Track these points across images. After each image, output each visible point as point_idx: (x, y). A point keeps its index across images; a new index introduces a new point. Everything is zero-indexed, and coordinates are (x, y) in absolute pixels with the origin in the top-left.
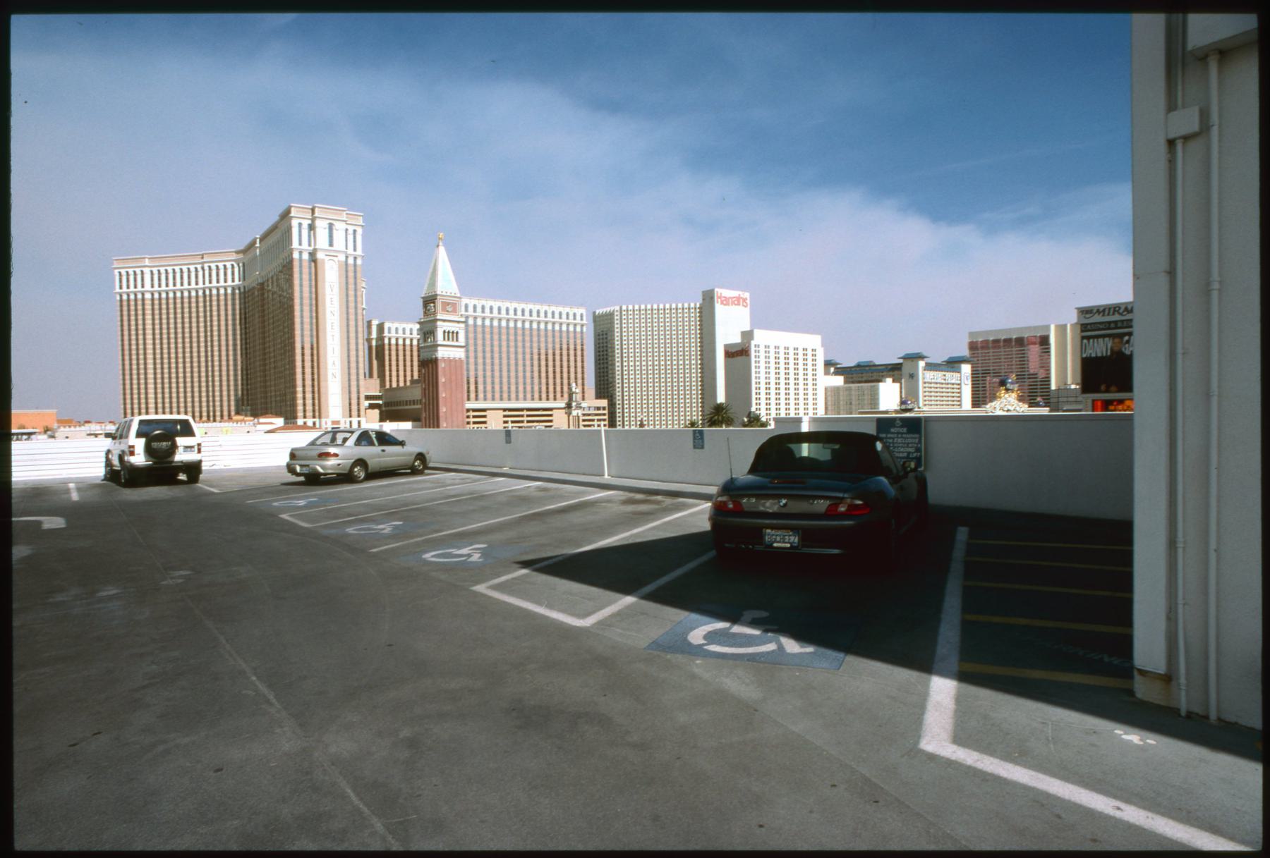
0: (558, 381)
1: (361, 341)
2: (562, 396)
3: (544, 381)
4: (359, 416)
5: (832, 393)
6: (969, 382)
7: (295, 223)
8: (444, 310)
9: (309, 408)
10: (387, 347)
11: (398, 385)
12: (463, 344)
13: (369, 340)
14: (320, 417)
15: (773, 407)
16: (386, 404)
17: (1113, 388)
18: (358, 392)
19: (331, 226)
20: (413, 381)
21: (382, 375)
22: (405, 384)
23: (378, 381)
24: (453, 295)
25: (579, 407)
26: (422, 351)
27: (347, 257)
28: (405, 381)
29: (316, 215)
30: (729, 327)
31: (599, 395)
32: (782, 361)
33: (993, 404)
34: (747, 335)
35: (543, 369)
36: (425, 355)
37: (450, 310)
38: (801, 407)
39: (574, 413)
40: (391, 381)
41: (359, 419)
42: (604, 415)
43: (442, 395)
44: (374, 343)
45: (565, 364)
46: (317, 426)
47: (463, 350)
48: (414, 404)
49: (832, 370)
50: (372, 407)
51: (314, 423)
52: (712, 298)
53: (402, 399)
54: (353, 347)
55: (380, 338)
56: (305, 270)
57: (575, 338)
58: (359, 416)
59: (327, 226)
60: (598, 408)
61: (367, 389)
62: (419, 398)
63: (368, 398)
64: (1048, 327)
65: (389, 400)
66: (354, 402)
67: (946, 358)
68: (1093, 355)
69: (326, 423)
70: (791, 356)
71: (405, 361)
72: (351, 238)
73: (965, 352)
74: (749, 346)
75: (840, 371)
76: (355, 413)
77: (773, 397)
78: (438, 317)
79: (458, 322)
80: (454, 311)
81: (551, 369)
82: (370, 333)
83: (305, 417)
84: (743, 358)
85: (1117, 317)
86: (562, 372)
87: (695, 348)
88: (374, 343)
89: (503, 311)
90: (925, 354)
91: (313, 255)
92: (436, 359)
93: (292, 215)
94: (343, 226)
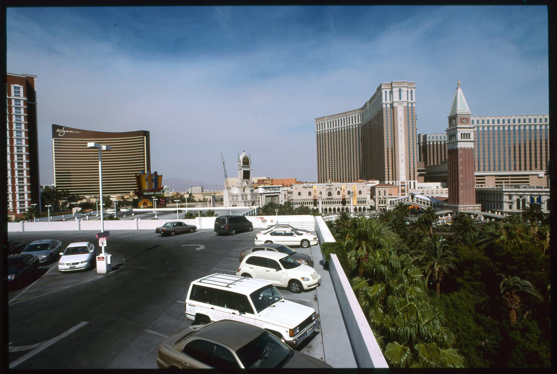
0: (528, 159)
1: (415, 143)
2: (536, 167)
4: (414, 180)
7: (383, 91)
8: (462, 122)
10: (428, 146)
12: (473, 140)
14: (396, 180)
18: (414, 168)
20: (441, 162)
23: (424, 163)
24: (467, 113)
28: (437, 162)
36: (452, 147)
40: (430, 162)
41: (414, 181)
44: (422, 145)
46: (394, 184)
47: (473, 143)
48: (442, 173)
50: (420, 175)
51: (393, 183)
55: (425, 142)
56: (389, 112)
61: (418, 167)
62: (447, 170)
69: (398, 183)
72: (410, 94)
76: (412, 178)
78: (458, 126)
79: (470, 128)
82: (419, 140)
83: (389, 180)
88: (422, 145)
91: (392, 105)
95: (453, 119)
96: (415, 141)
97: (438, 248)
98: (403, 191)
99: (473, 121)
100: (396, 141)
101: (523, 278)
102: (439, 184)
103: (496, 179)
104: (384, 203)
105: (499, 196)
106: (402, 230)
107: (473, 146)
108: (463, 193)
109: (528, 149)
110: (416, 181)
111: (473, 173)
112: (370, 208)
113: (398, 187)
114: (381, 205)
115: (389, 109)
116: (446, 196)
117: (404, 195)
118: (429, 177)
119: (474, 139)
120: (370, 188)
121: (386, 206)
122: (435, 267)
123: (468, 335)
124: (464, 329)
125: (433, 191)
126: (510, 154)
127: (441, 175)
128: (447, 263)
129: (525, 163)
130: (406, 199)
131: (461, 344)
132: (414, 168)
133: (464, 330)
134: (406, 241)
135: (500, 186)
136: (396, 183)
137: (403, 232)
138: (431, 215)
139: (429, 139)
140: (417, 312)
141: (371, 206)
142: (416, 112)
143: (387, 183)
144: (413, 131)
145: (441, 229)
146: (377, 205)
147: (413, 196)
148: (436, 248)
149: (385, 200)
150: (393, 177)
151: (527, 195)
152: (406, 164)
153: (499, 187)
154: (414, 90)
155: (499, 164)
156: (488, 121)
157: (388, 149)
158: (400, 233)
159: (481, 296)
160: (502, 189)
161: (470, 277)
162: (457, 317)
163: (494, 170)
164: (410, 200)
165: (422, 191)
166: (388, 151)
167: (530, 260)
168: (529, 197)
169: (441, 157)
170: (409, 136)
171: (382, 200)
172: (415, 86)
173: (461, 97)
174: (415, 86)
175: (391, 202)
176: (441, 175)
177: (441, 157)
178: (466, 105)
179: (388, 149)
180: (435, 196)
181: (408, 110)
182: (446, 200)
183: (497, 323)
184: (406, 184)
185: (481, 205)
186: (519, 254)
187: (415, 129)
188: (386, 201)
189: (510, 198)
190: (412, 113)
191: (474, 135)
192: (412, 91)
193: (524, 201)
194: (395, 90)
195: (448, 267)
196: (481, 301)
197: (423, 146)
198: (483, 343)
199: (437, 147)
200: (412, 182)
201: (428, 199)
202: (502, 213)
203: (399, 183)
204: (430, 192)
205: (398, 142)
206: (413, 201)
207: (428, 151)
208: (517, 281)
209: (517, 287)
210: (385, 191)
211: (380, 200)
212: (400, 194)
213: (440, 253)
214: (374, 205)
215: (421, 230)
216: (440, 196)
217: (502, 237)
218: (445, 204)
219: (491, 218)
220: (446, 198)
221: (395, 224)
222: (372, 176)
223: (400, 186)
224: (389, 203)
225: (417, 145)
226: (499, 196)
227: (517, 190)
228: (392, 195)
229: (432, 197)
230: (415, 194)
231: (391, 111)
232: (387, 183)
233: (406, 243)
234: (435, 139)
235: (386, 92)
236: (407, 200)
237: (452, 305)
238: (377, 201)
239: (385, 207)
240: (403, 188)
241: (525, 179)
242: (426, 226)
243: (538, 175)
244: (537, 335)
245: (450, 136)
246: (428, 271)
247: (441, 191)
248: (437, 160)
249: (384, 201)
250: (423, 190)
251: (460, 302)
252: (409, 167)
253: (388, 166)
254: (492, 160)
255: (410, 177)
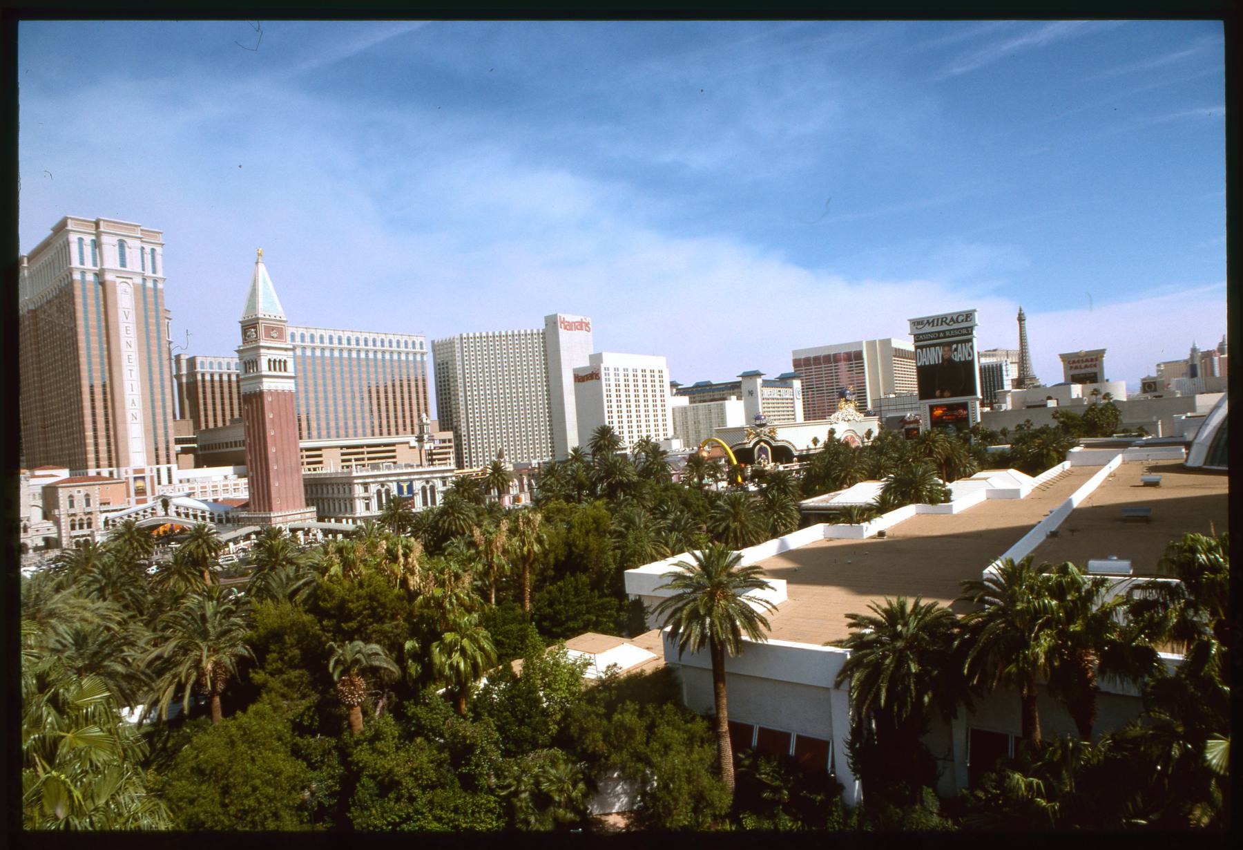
0: (392, 414)
1: (167, 377)
2: (405, 430)
3: (384, 414)
4: (169, 462)
5: (680, 413)
6: (801, 397)
7: (73, 238)
8: (268, 335)
9: (103, 455)
10: (200, 384)
11: (216, 425)
12: (293, 375)
13: (178, 377)
14: (118, 466)
15: (635, 429)
16: (203, 447)
17: (947, 393)
18: (166, 435)
19: (122, 244)
20: (233, 420)
21: (195, 417)
22: (224, 424)
23: (191, 422)
24: (278, 318)
25: (432, 439)
26: (241, 383)
27: (144, 280)
28: (224, 421)
29: (102, 229)
30: (574, 355)
31: (444, 427)
32: (631, 383)
33: (836, 414)
34: (596, 358)
35: (383, 402)
36: (246, 388)
37: (275, 335)
38: (652, 428)
39: (427, 446)
40: (207, 421)
42: (450, 447)
43: (271, 433)
44: (184, 380)
45: (406, 396)
46: (115, 476)
47: (293, 381)
48: (236, 446)
49: (674, 391)
50: (184, 451)
51: (111, 473)
52: (555, 323)
53: (217, 441)
54: (157, 382)
55: (192, 373)
56: (91, 295)
57: (415, 368)
58: (169, 462)
59: (117, 243)
60: (444, 441)
61: (177, 431)
62: (243, 438)
63: (178, 441)
64: (861, 343)
65: (204, 443)
66: (162, 446)
67: (778, 375)
68: (927, 363)
69: (126, 472)
70: (640, 378)
71: (214, 404)
72: (148, 258)
73: (790, 369)
74: (599, 369)
75: (682, 392)
76: (163, 458)
77: (634, 419)
78: (261, 344)
79: (286, 349)
80: (281, 336)
81: (391, 402)
82: (179, 368)
84: (594, 381)
85: (945, 327)
86: (403, 405)
87: (540, 375)
88: (184, 380)
89: (336, 341)
90: (762, 372)
91: (99, 275)
92: (261, 393)
93: (69, 227)
94: (138, 243)
95: (249, 327)
96: (166, 370)
97: (211, 617)
98: (140, 492)
99: (293, 336)
100: (115, 369)
101: (367, 640)
102: (229, 470)
103: (343, 454)
104: (85, 526)
105: (346, 487)
106: (128, 590)
107: (293, 388)
108: (279, 488)
109: (390, 395)
110: (174, 467)
111: (296, 444)
112: (42, 544)
113: (127, 484)
114: (78, 532)
115: (93, 287)
116: (244, 495)
117: (145, 501)
118: (207, 456)
119: (296, 371)
120: (40, 491)
121: (92, 535)
122: (204, 664)
123: (276, 789)
124: (267, 781)
125: (216, 486)
126: (362, 405)
127: (234, 449)
128: (230, 646)
129: (404, 422)
130: (149, 510)
131: (265, 815)
132: (166, 435)
133: (267, 783)
134: (142, 614)
135: (348, 467)
136: (119, 473)
137: (131, 594)
138: (205, 541)
139: (202, 368)
140: (70, 792)
141: (47, 540)
142: (168, 301)
143: (94, 474)
144: (159, 346)
145: (235, 572)
146: (64, 535)
147: (165, 504)
148: (203, 618)
149: (89, 519)
150: (110, 459)
151: (391, 481)
152: (145, 426)
153: (346, 470)
154: (159, 250)
155: (328, 424)
156: (322, 338)
157: (92, 387)
158: (123, 597)
159: (304, 697)
160: (351, 472)
161: (279, 664)
162: (253, 760)
163: (319, 437)
164: (160, 511)
165: (190, 489)
166: (92, 393)
167: (375, 604)
168: (395, 484)
169: (232, 409)
170: (150, 359)
171: (81, 519)
172: (161, 239)
173: (264, 280)
174: (161, 239)
175: (106, 523)
176: (234, 449)
177: (232, 409)
178: (277, 301)
179: (92, 387)
180: (221, 497)
181: (145, 297)
182: (245, 506)
183: (333, 742)
184: (147, 474)
185: (315, 509)
186: (359, 598)
187: (164, 343)
188: (93, 521)
189: (366, 490)
190: (156, 304)
191: (295, 363)
192: (153, 250)
193: (433, 489)
194: (109, 242)
195: (235, 655)
196: (301, 709)
197: (187, 384)
198: (307, 794)
199: (221, 387)
200: (164, 468)
201: (204, 507)
202: (354, 522)
203: (127, 472)
204: (209, 490)
205: (121, 375)
206: (167, 514)
207: (201, 396)
208: (358, 649)
209: (357, 661)
210: (87, 495)
211: (73, 520)
212: (133, 498)
213: (214, 627)
214: (55, 536)
215: (183, 580)
216: (232, 497)
217: (333, 570)
218: (244, 514)
219: (335, 532)
220: (242, 500)
221: (108, 577)
222: (47, 458)
223: (131, 481)
224: (102, 525)
225: (172, 382)
226: (346, 487)
227: (376, 472)
228: (109, 503)
229: (215, 501)
230: (171, 498)
231: (97, 291)
232: (94, 474)
233: (142, 621)
234: (216, 369)
235: (81, 240)
236: (152, 514)
237: (242, 736)
238: (65, 522)
239: (89, 535)
240: (140, 483)
241: (387, 452)
242: (193, 571)
243: (408, 443)
244: (394, 738)
245: (245, 363)
246: (188, 676)
247: (235, 485)
248: (224, 415)
249: (77, 523)
250: (192, 486)
251: (259, 724)
252: (152, 430)
253: (95, 430)
254: (332, 416)
255: (157, 456)
